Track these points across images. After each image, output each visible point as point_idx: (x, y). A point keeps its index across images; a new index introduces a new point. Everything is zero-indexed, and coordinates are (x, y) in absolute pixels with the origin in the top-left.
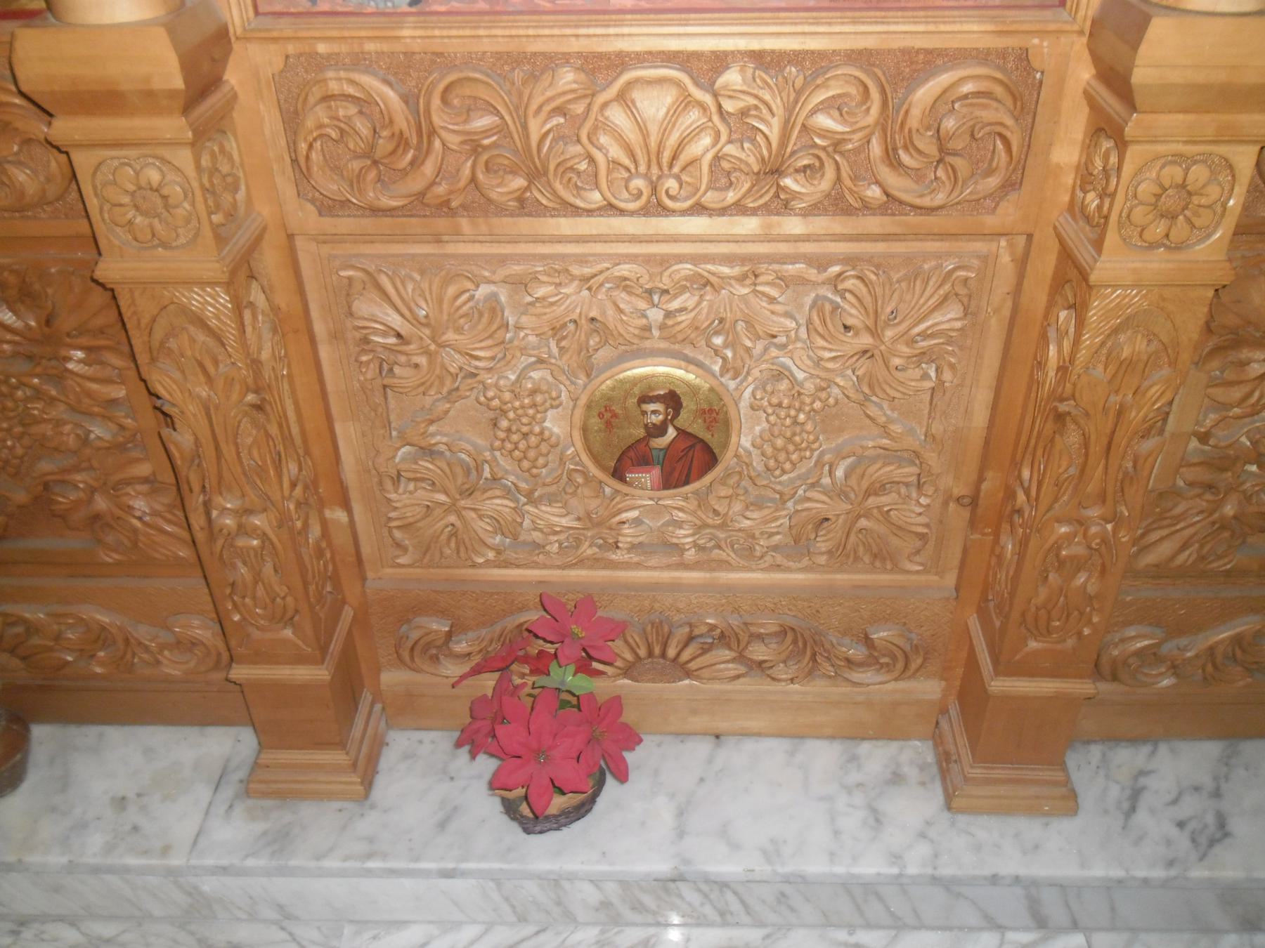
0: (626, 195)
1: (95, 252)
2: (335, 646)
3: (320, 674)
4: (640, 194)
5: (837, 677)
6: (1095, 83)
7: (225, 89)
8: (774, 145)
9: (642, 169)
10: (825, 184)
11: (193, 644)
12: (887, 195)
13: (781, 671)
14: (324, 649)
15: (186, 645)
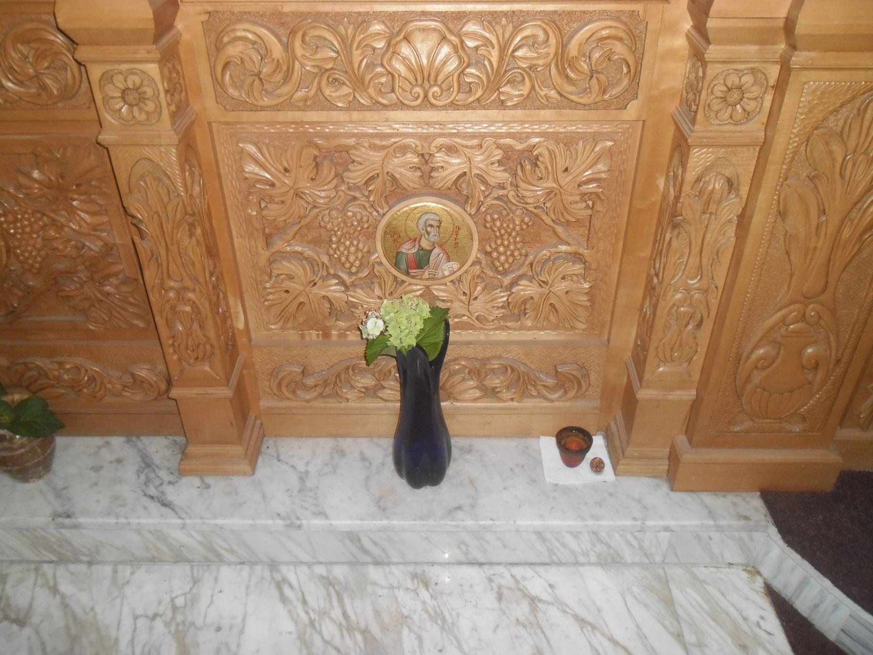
0: (411, 97)
1: (99, 126)
2: (234, 380)
3: (227, 392)
4: (417, 98)
5: (540, 396)
6: (693, 32)
7: (173, 32)
8: (495, 66)
9: (420, 82)
10: (525, 89)
11: (143, 382)
12: (561, 95)
13: (506, 395)
14: (228, 381)
15: (138, 383)
